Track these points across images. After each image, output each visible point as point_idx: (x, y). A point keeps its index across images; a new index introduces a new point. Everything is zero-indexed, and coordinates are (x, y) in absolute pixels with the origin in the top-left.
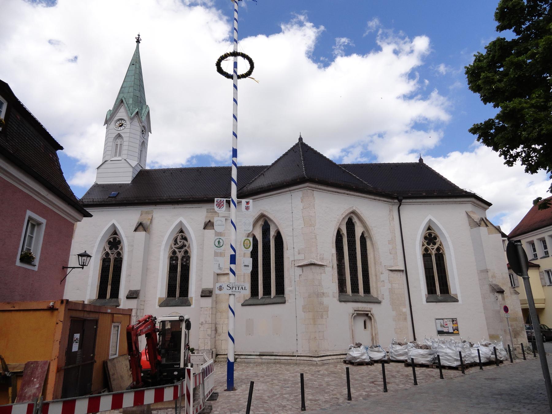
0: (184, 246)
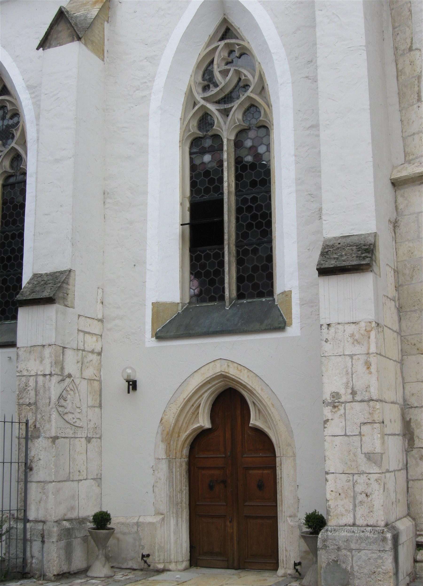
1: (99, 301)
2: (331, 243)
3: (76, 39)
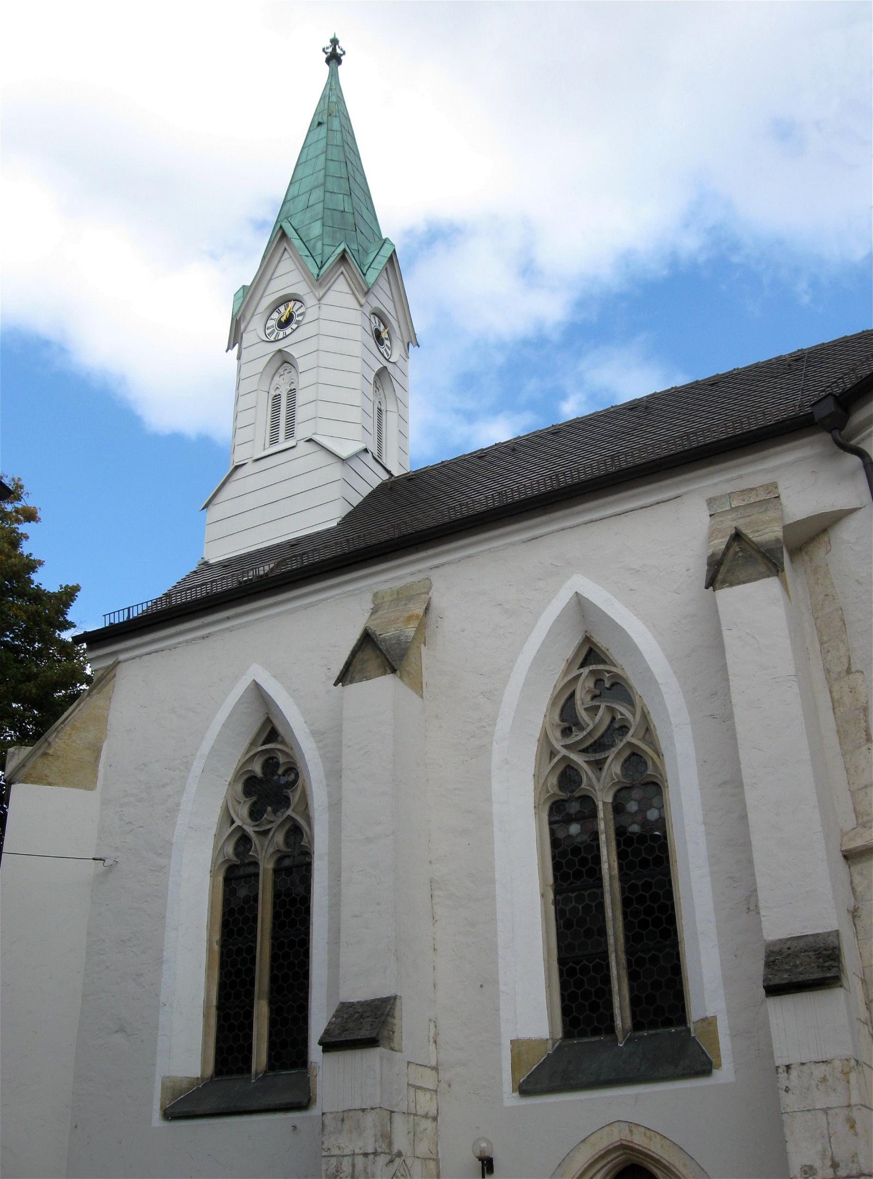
0: (620, 728)
1: (432, 1041)
2: (777, 948)
3: (389, 671)
